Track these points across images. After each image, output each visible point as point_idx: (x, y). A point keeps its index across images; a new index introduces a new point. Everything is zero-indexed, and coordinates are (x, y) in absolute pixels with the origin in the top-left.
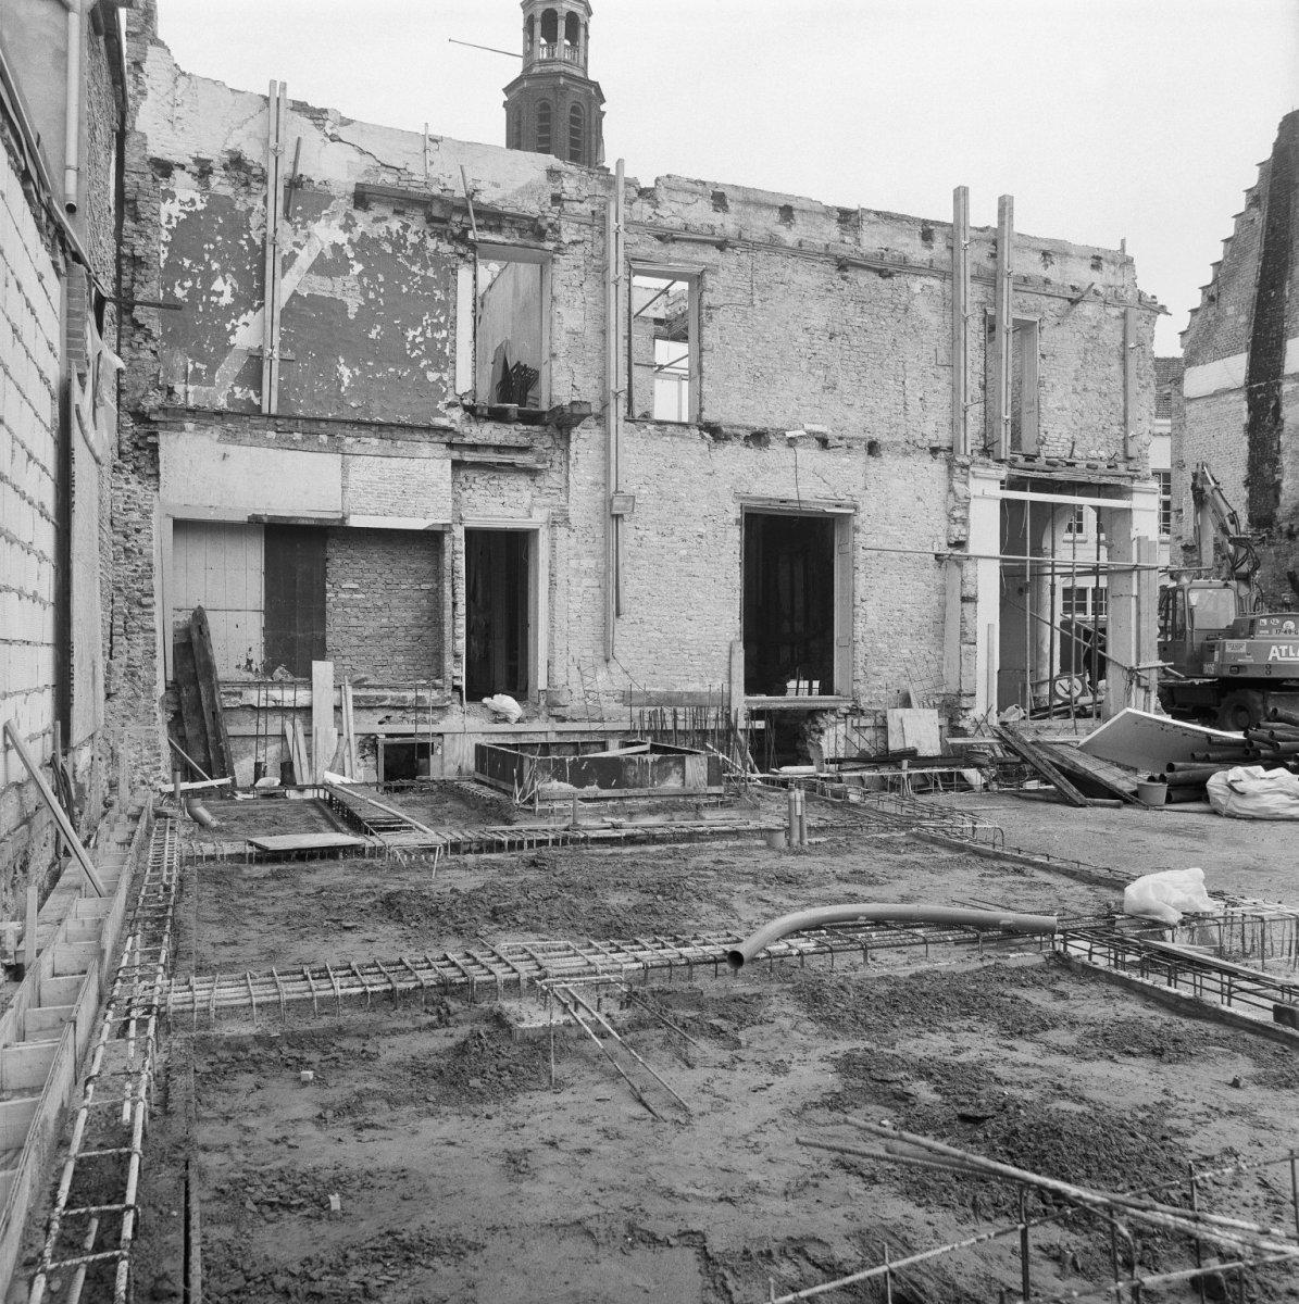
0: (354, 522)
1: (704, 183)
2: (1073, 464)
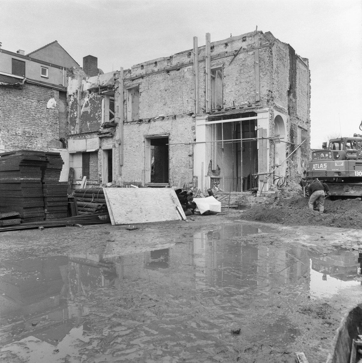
0: (87, 151)
1: (139, 64)
2: (235, 109)
